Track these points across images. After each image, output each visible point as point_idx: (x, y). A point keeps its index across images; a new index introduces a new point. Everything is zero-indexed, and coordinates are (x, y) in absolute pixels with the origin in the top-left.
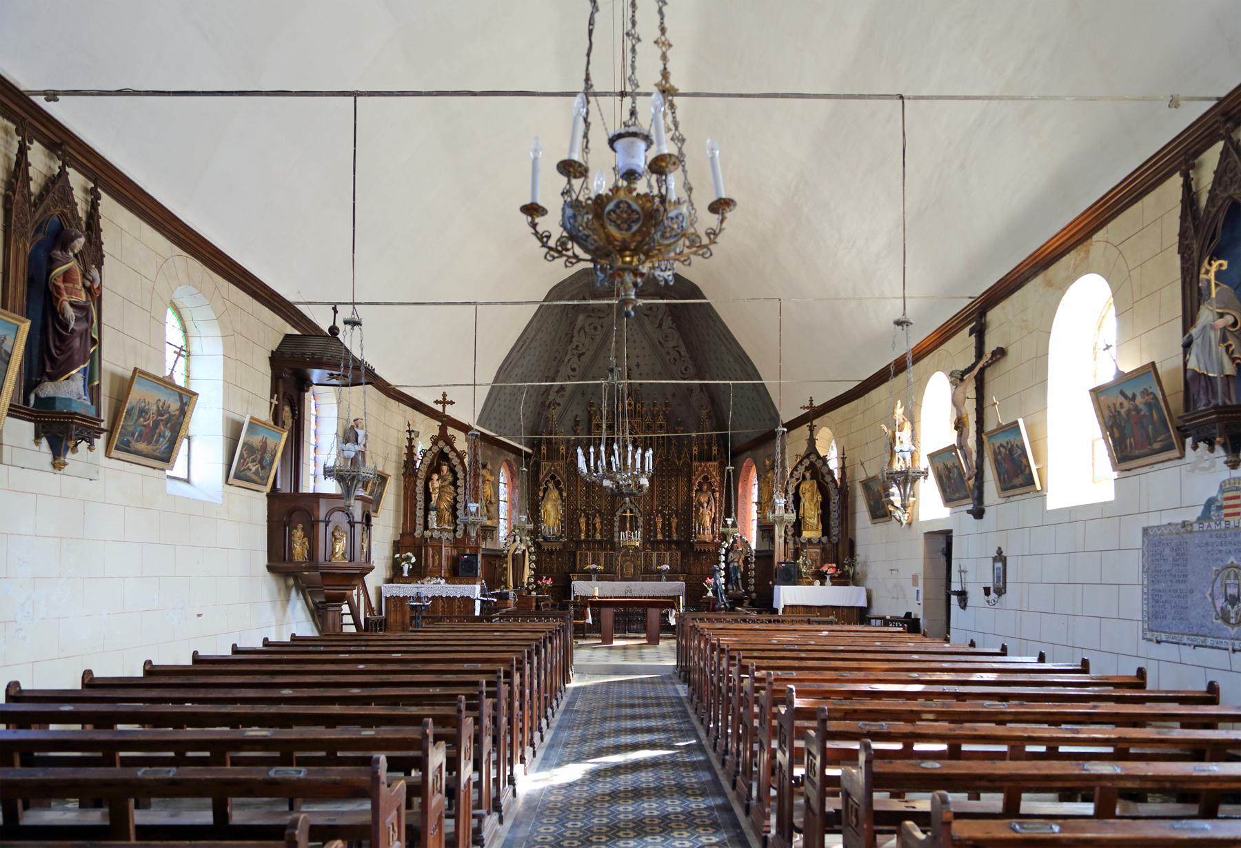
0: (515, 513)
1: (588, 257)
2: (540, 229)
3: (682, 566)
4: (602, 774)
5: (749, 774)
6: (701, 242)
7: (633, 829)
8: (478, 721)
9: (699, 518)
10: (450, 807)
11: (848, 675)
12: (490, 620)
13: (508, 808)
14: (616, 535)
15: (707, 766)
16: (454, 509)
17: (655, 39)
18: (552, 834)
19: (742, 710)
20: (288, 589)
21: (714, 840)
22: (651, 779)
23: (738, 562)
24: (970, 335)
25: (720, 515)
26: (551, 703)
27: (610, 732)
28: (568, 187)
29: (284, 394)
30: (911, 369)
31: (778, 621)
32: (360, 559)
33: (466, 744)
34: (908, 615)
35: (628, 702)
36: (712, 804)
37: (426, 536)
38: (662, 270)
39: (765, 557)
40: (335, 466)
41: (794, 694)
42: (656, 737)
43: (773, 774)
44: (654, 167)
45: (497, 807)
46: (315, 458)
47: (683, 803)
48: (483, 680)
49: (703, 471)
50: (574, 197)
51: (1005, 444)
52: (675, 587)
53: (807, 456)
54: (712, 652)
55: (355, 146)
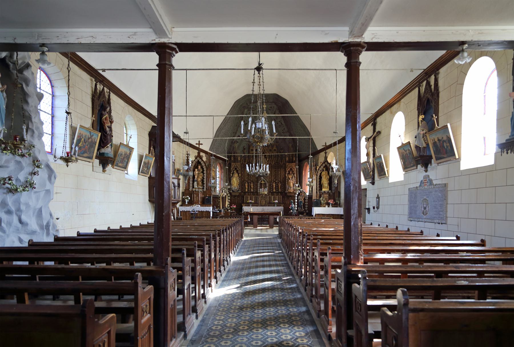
0: (222, 182)
3: (282, 201)
14: (259, 190)
15: (284, 256)
23: (302, 199)
35: (262, 243)
39: (310, 197)
49: (290, 167)
52: (280, 209)
53: (324, 163)
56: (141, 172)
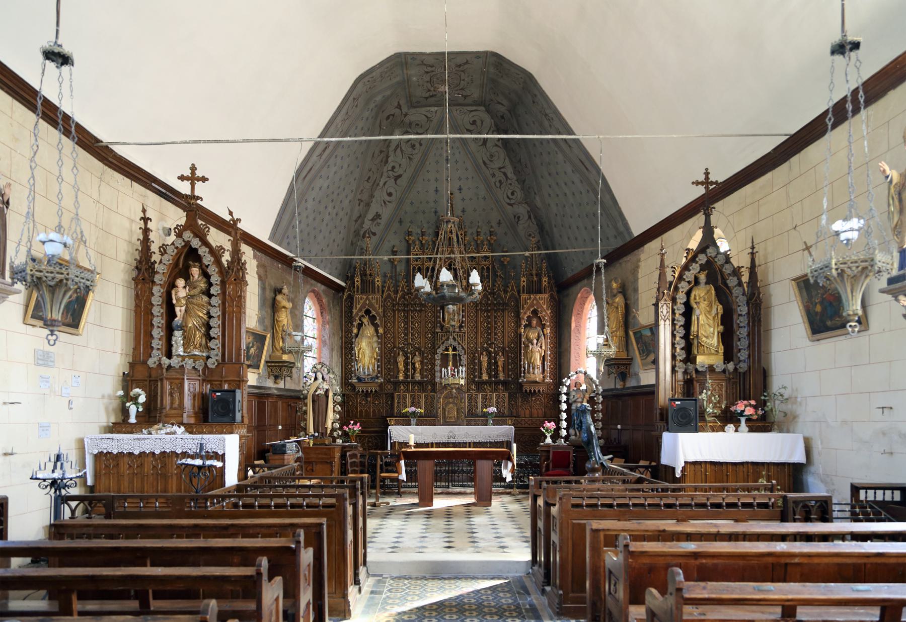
3: (509, 409)
9: (529, 356)
14: (437, 374)
49: (532, 305)
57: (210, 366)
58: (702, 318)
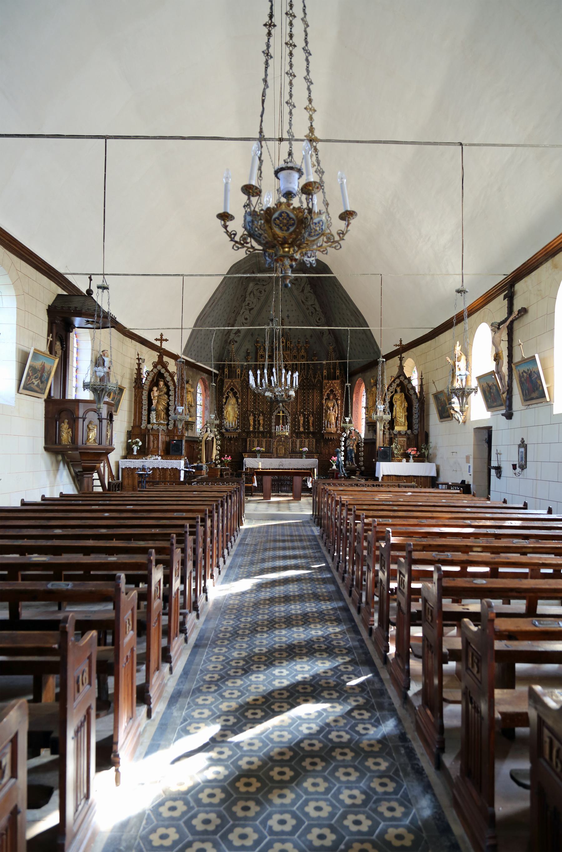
0: (207, 413)
1: (261, 248)
2: (229, 229)
4: (264, 586)
5: (360, 586)
6: (334, 239)
7: (284, 623)
8: (184, 551)
10: (164, 608)
11: (425, 522)
12: (190, 483)
13: (203, 608)
14: (273, 428)
15: (333, 581)
16: (167, 410)
17: (305, 106)
18: (231, 626)
19: (356, 544)
20: (58, 462)
21: (337, 630)
22: (296, 590)
23: (352, 446)
24: (504, 299)
25: (341, 415)
26: (231, 539)
27: (269, 558)
28: (248, 202)
29: (57, 333)
30: (467, 320)
31: (379, 486)
32: (105, 443)
33: (176, 566)
34: (463, 482)
35: (281, 538)
36: (336, 606)
37: (149, 428)
38: (308, 257)
40: (90, 382)
41: (391, 534)
42: (299, 561)
43: (376, 586)
44: (304, 189)
45: (195, 608)
46: (76, 376)
47: (317, 605)
48: (187, 523)
50: (252, 209)
51: (526, 371)
52: (312, 462)
53: (398, 377)
54: (336, 505)
55: (105, 172)
56: (25, 388)
57: (169, 428)
58: (398, 408)
